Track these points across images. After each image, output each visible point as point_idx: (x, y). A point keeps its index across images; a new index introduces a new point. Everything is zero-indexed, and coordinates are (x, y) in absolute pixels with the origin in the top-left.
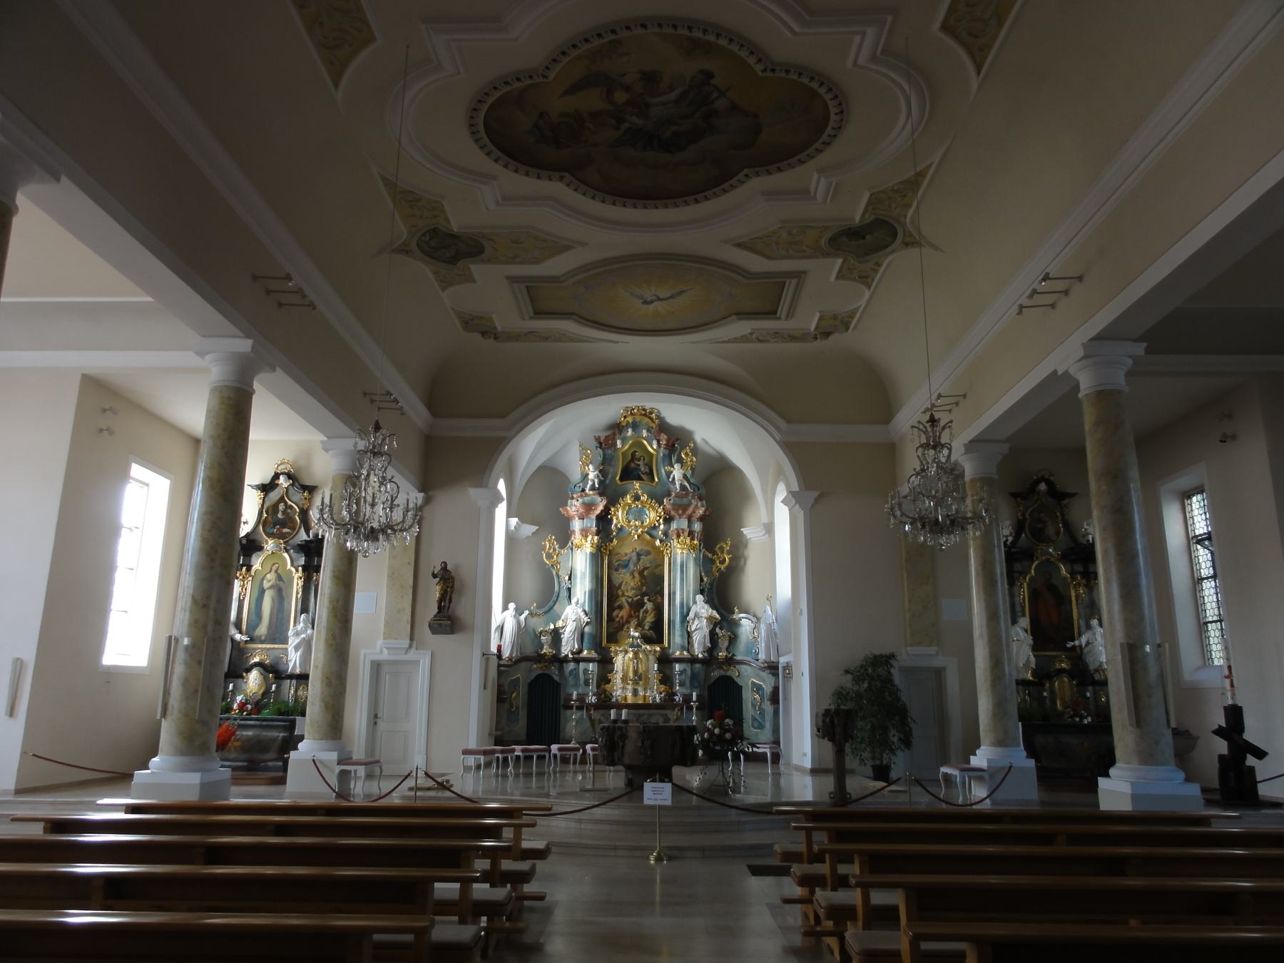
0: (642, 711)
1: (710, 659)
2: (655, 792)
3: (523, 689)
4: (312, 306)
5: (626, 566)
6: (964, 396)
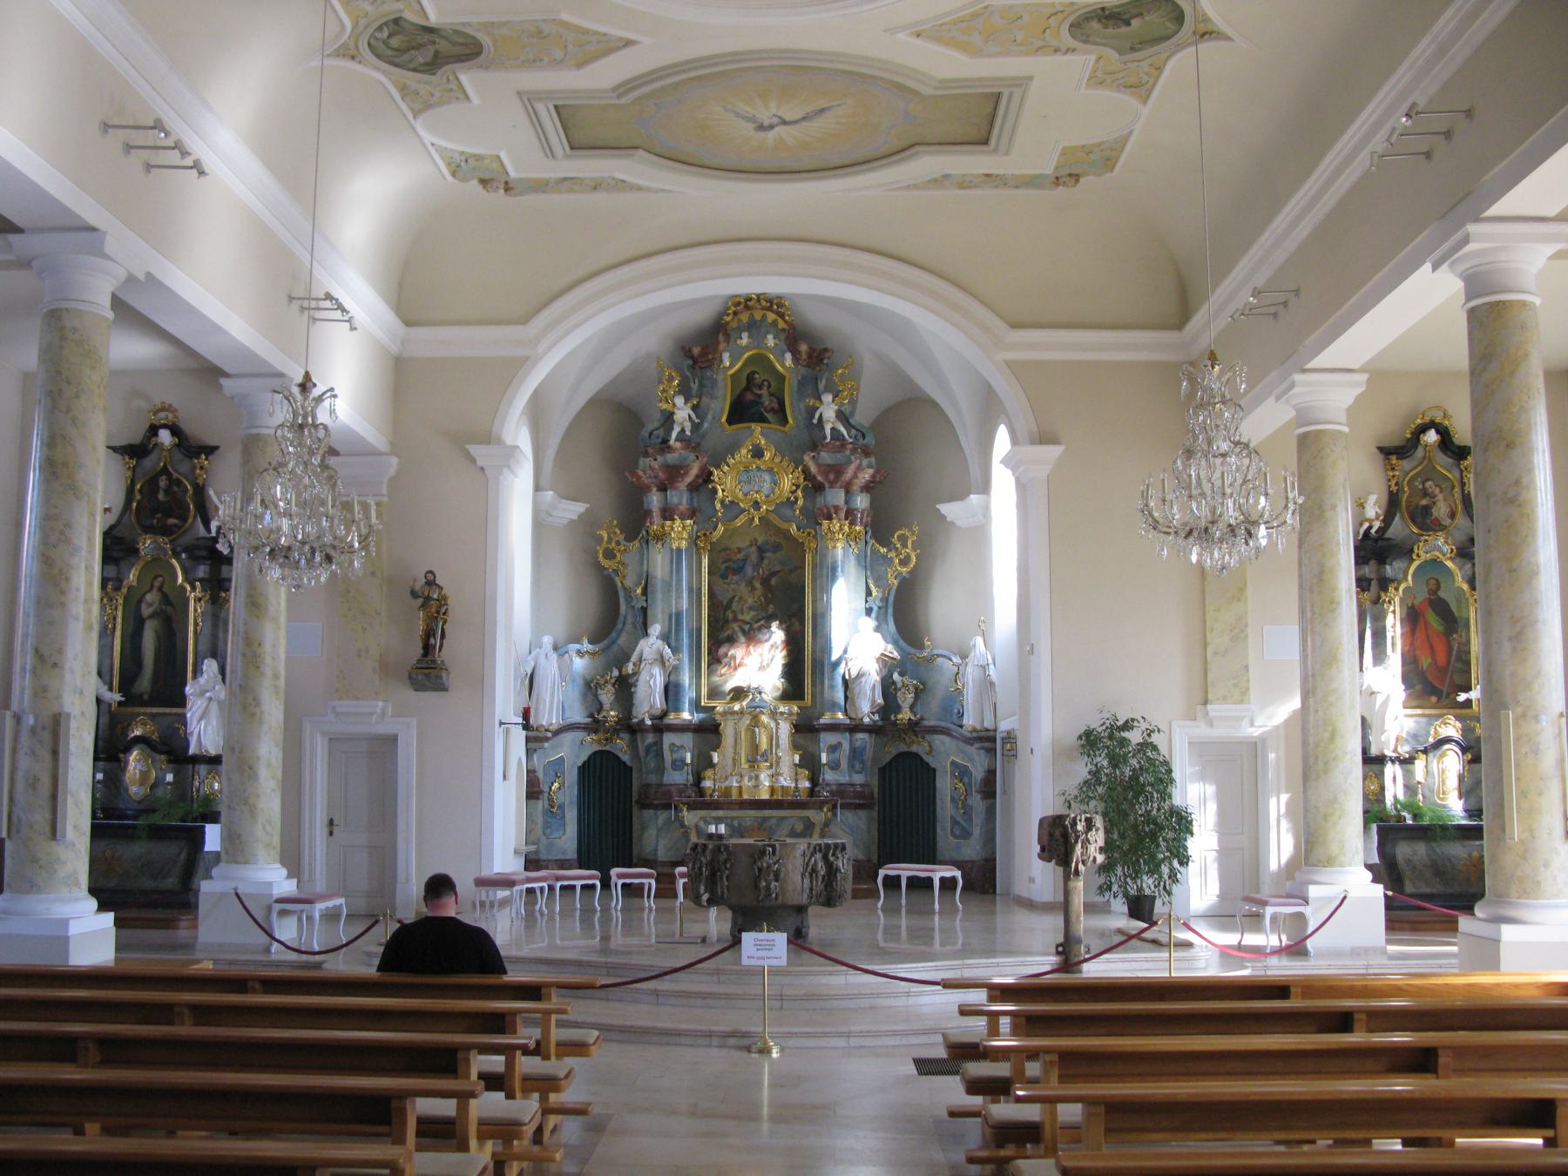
0: (767, 813)
1: (886, 725)
2: (759, 945)
3: (572, 777)
4: (198, 167)
5: (739, 570)
6: (1297, 292)
